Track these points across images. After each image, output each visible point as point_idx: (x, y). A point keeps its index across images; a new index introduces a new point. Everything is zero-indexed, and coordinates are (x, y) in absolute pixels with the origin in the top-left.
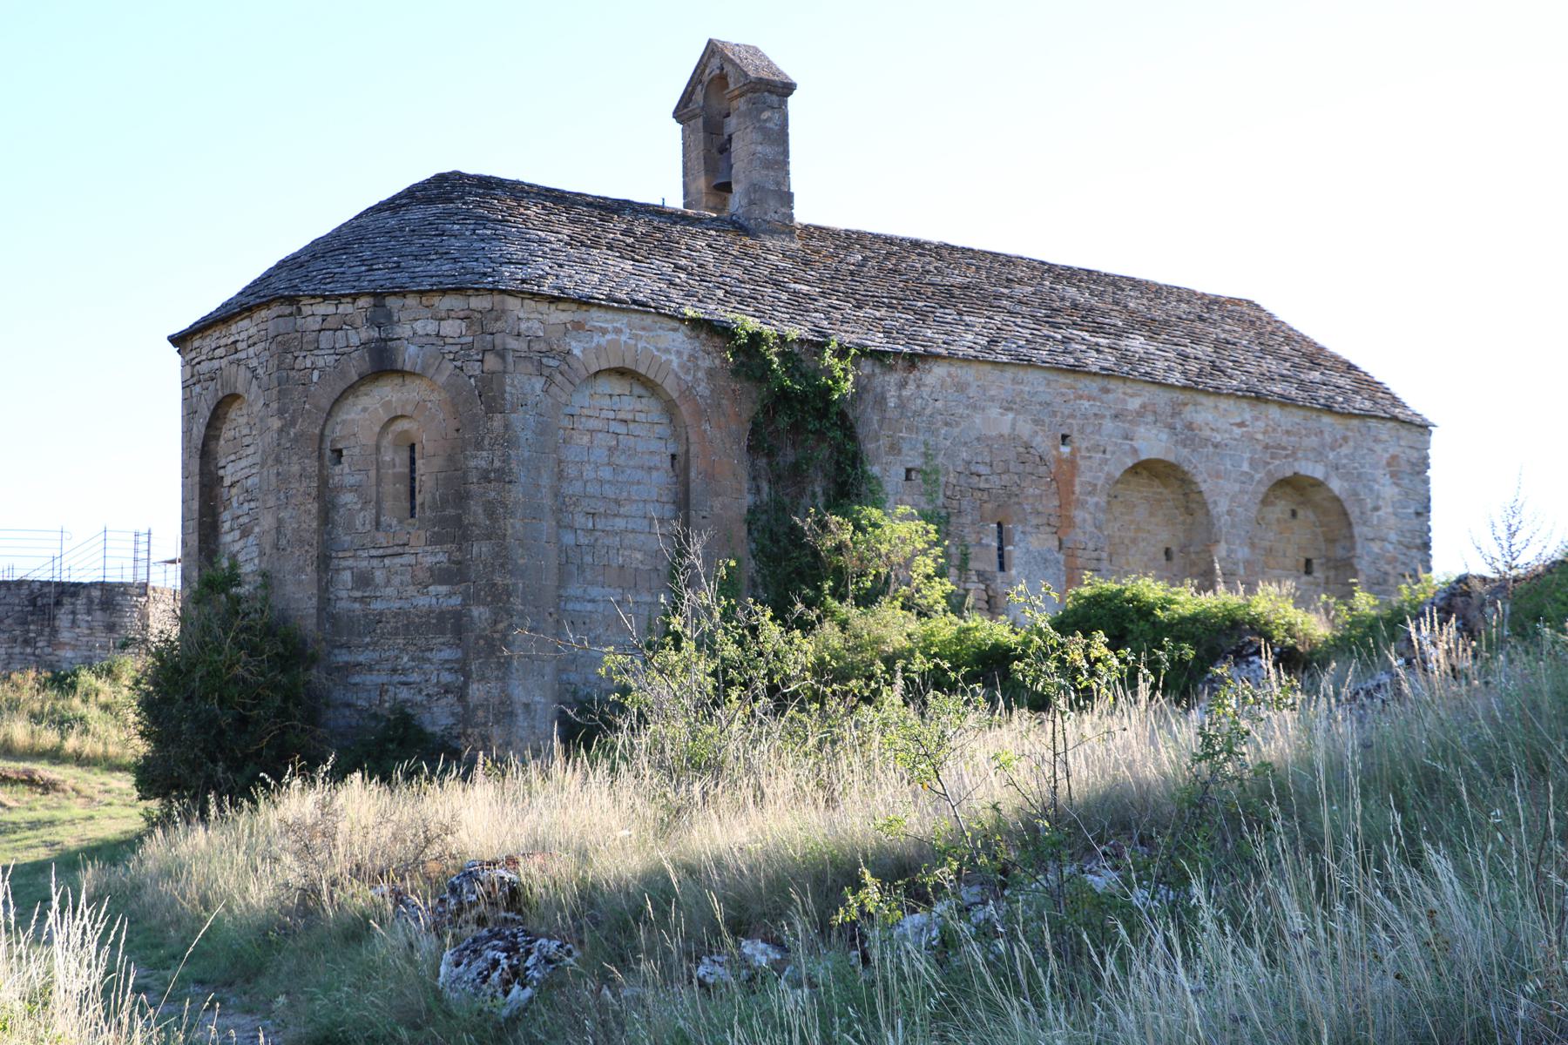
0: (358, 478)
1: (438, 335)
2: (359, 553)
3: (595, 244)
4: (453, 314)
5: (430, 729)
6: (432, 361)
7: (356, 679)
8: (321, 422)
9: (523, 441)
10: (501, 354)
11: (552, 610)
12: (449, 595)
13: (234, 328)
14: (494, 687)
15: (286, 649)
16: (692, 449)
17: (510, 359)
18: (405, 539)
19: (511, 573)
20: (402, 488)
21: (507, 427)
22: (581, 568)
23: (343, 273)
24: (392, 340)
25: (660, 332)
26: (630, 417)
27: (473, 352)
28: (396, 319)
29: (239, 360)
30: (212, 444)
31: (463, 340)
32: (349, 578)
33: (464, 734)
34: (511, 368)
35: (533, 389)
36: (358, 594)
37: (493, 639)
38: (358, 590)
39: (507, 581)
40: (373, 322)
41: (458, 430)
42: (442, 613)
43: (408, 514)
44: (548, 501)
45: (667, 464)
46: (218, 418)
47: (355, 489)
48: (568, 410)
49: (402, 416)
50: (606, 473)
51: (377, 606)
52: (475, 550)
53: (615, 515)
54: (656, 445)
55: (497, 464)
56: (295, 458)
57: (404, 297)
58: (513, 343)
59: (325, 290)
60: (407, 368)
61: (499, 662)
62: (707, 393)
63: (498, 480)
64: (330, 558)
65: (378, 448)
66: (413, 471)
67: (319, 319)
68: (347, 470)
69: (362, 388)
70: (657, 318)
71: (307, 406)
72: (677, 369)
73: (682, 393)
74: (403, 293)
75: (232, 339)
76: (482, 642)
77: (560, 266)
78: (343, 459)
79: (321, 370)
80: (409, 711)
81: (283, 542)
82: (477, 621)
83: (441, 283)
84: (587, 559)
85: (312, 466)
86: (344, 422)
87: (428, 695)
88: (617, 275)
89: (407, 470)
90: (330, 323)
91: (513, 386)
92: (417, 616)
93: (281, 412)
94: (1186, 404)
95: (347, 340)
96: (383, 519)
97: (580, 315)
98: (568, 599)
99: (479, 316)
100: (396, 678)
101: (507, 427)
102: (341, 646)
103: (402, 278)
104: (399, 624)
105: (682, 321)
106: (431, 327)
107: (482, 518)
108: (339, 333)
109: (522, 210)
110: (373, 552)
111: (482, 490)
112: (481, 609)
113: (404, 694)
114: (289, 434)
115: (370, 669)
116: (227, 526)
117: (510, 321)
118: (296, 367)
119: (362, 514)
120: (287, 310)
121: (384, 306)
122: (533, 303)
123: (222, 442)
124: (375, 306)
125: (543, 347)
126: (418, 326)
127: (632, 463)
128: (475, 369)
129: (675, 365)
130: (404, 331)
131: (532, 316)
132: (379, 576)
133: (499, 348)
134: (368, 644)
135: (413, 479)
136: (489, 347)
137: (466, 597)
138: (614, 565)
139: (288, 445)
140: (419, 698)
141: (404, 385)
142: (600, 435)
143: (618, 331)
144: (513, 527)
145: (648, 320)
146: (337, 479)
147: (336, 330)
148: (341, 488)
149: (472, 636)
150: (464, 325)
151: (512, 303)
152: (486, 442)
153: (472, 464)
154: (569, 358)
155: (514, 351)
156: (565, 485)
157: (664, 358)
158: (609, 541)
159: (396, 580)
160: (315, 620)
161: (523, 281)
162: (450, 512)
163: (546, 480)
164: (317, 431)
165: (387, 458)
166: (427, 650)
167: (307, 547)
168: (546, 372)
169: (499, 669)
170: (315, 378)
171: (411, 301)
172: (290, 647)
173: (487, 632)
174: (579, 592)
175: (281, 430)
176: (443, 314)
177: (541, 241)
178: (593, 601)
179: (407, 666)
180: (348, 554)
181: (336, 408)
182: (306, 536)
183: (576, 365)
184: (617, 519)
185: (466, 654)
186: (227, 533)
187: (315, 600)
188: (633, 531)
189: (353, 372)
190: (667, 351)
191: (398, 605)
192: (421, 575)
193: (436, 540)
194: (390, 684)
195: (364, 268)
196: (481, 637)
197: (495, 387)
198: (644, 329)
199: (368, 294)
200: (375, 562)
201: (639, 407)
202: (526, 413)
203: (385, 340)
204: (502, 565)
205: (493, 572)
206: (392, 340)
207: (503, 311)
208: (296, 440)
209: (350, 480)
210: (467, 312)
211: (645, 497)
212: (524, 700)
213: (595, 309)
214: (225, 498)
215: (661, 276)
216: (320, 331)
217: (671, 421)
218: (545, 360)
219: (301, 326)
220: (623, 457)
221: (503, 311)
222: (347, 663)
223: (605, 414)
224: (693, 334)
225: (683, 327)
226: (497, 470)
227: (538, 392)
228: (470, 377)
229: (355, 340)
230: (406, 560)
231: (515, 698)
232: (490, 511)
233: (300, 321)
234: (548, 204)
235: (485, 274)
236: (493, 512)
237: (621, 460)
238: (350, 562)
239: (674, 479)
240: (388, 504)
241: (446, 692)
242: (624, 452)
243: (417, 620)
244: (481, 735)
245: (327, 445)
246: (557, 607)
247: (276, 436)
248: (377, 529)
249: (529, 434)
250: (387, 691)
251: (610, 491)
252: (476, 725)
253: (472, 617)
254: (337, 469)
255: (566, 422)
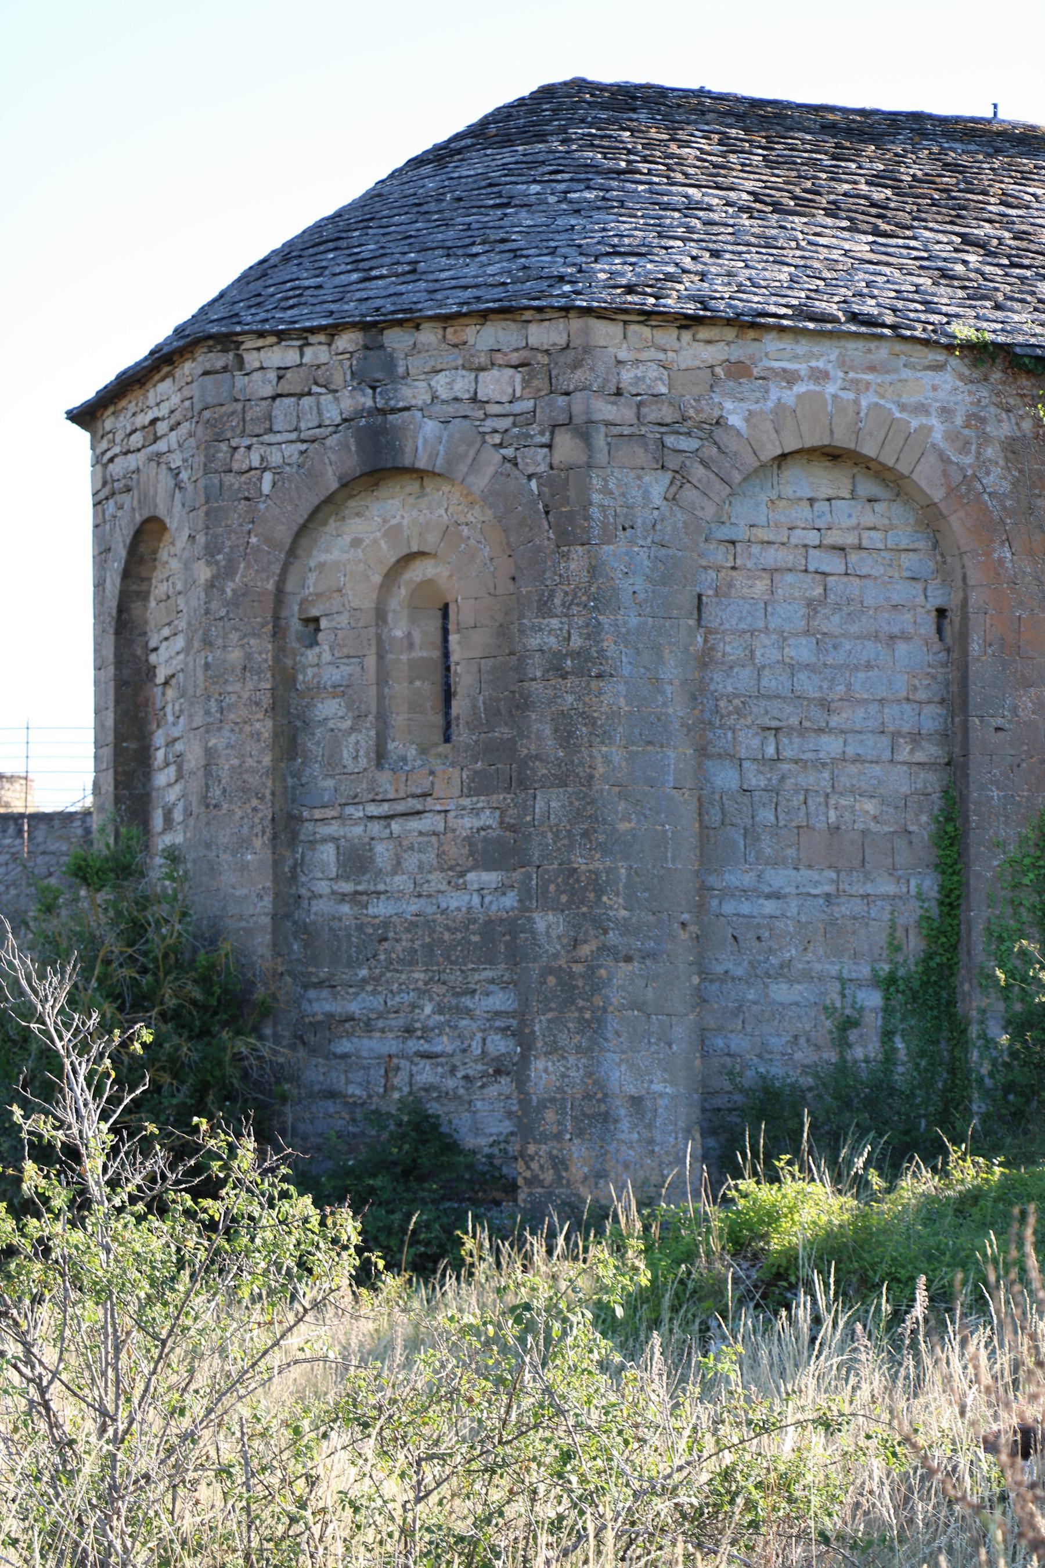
0: (346, 670)
1: (474, 399)
2: (349, 810)
3: (804, 205)
4: (499, 358)
5: (470, 1142)
6: (462, 449)
7: (344, 1046)
8: (277, 568)
9: (626, 597)
10: (584, 433)
11: (686, 917)
12: (502, 889)
13: (152, 397)
14: (575, 1067)
15: (210, 993)
16: (973, 597)
17: (600, 440)
18: (425, 784)
19: (604, 849)
20: (428, 688)
21: (593, 571)
22: (751, 834)
23: (319, 287)
24: (394, 411)
25: (906, 373)
26: (850, 539)
27: (533, 430)
28: (401, 370)
29: (159, 455)
30: (136, 608)
31: (518, 407)
32: (333, 858)
33: (522, 1154)
34: (601, 457)
35: (646, 495)
36: (347, 887)
37: (572, 976)
38: (347, 879)
39: (597, 865)
40: (362, 379)
41: (514, 579)
42: (489, 923)
43: (438, 736)
44: (677, 710)
45: (928, 627)
46: (141, 561)
47: (341, 690)
48: (724, 532)
49: (421, 554)
50: (802, 651)
51: (380, 909)
52: (540, 805)
53: (821, 731)
54: (902, 592)
55: (577, 642)
56: (234, 636)
57: (417, 327)
58: (605, 410)
59: (282, 321)
60: (422, 463)
61: (581, 1020)
62: (1005, 486)
63: (580, 672)
64: (301, 820)
65: (380, 615)
66: (446, 654)
67: (272, 375)
68: (327, 657)
69: (351, 503)
70: (899, 347)
71: (253, 540)
72: (942, 445)
73: (951, 490)
74: (411, 320)
75: (150, 416)
76: (552, 980)
77: (716, 254)
78: (321, 636)
79: (277, 471)
80: (433, 1108)
81: (216, 792)
82: (542, 939)
83: (478, 299)
84: (766, 815)
85: (262, 649)
86: (321, 566)
87: (466, 1077)
88: (831, 264)
89: (436, 654)
90: (293, 382)
91: (606, 491)
92: (448, 928)
93: (211, 551)
94: (841, 700)
95: (320, 413)
96: (391, 746)
97: (742, 349)
98: (727, 893)
99: (544, 359)
100: (413, 1045)
101: (593, 571)
102: (320, 985)
103: (414, 293)
104: (417, 945)
105: (949, 348)
106: (463, 384)
107: (551, 747)
108: (306, 401)
109: (674, 148)
110: (373, 810)
111: (550, 692)
112: (551, 917)
113: (426, 1074)
114: (223, 591)
115: (369, 1027)
116: (160, 755)
117: (601, 367)
118: (236, 467)
119: (352, 739)
120: (219, 360)
121: (382, 347)
122: (646, 331)
123: (153, 604)
124: (366, 348)
125: (667, 414)
126: (440, 382)
127: (854, 629)
128: (536, 460)
129: (937, 436)
130: (415, 393)
131: (644, 356)
132: (383, 852)
133: (578, 420)
134: (364, 981)
135: (448, 669)
136: (562, 418)
137: (525, 895)
138: (821, 826)
139: (223, 612)
140: (450, 1083)
141: (422, 495)
142: (789, 578)
143: (820, 376)
144: (607, 761)
145: (882, 352)
146: (310, 672)
147: (301, 395)
148: (317, 690)
149: (535, 969)
150: (518, 377)
151: (604, 332)
152: (557, 601)
153: (534, 642)
154: (719, 433)
155: (608, 424)
156: (717, 676)
157: (914, 423)
158: (809, 779)
159: (411, 861)
160: (268, 937)
161: (630, 289)
162: (502, 732)
163: (672, 671)
164: (270, 586)
165: (399, 633)
166: (464, 993)
167: (255, 802)
168: (673, 462)
169: (581, 1032)
170: (266, 487)
171: (428, 336)
172: (217, 990)
173: (562, 962)
174: (748, 880)
175: (210, 585)
176: (483, 359)
177: (691, 207)
178: (776, 896)
179: (431, 1023)
180: (329, 813)
181: (304, 542)
182: (253, 780)
183: (732, 444)
184: (825, 739)
185: (525, 1002)
186: (161, 769)
187: (267, 901)
188: (858, 759)
189: (330, 473)
190: (921, 409)
191: (413, 908)
192: (456, 852)
193: (477, 786)
194: (403, 1056)
195: (355, 276)
196: (548, 971)
197: (572, 494)
198: (872, 369)
199: (354, 325)
200: (375, 828)
201: (868, 520)
202: (632, 542)
203: (383, 412)
204: (585, 834)
205: (570, 848)
206: (394, 411)
207: (587, 349)
208: (234, 603)
209: (332, 675)
210: (524, 354)
211: (882, 693)
212: (631, 1090)
213: (773, 335)
214: (159, 706)
215: (927, 262)
216: (274, 398)
217: (936, 544)
218: (670, 440)
219: (243, 389)
220: (836, 619)
221: (587, 349)
222: (330, 1016)
223: (799, 536)
224: (976, 375)
225: (954, 362)
226: (575, 655)
227: (657, 500)
228: (530, 477)
229: (332, 414)
230: (434, 822)
231: (614, 1087)
232: (566, 737)
233: (240, 381)
234: (733, 132)
235: (561, 279)
236: (571, 734)
237: (833, 624)
238: (334, 829)
239: (943, 656)
240: (399, 719)
241: (498, 1072)
242: (838, 607)
243: (447, 936)
244: (552, 1158)
245: (293, 612)
246: (701, 908)
247: (203, 595)
248: (379, 766)
249: (639, 584)
250: (398, 1069)
251: (809, 685)
252: (544, 1139)
253: (533, 932)
254: (311, 655)
255: (720, 556)
